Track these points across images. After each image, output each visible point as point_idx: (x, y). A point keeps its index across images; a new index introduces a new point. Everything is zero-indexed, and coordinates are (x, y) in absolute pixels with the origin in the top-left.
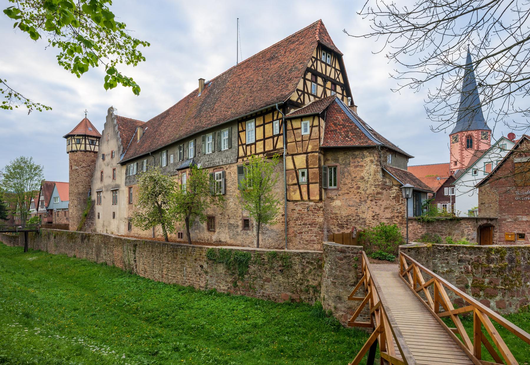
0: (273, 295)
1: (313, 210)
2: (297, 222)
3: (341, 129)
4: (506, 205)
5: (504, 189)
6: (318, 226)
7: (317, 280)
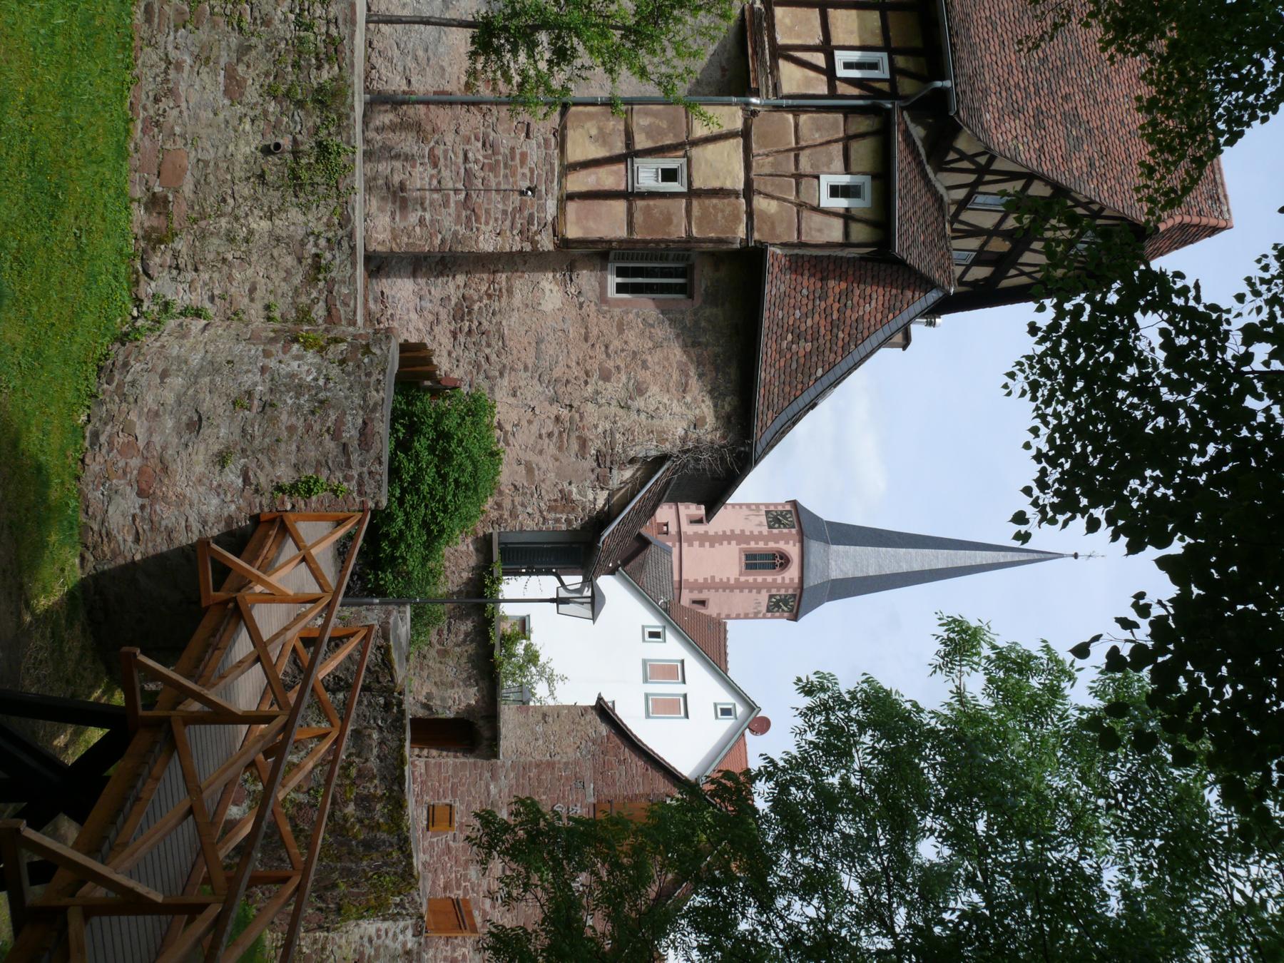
0: (175, 112)
1: (526, 213)
2: (480, 145)
3: (827, 313)
4: (539, 781)
5: (588, 774)
6: (462, 230)
7: (252, 300)
